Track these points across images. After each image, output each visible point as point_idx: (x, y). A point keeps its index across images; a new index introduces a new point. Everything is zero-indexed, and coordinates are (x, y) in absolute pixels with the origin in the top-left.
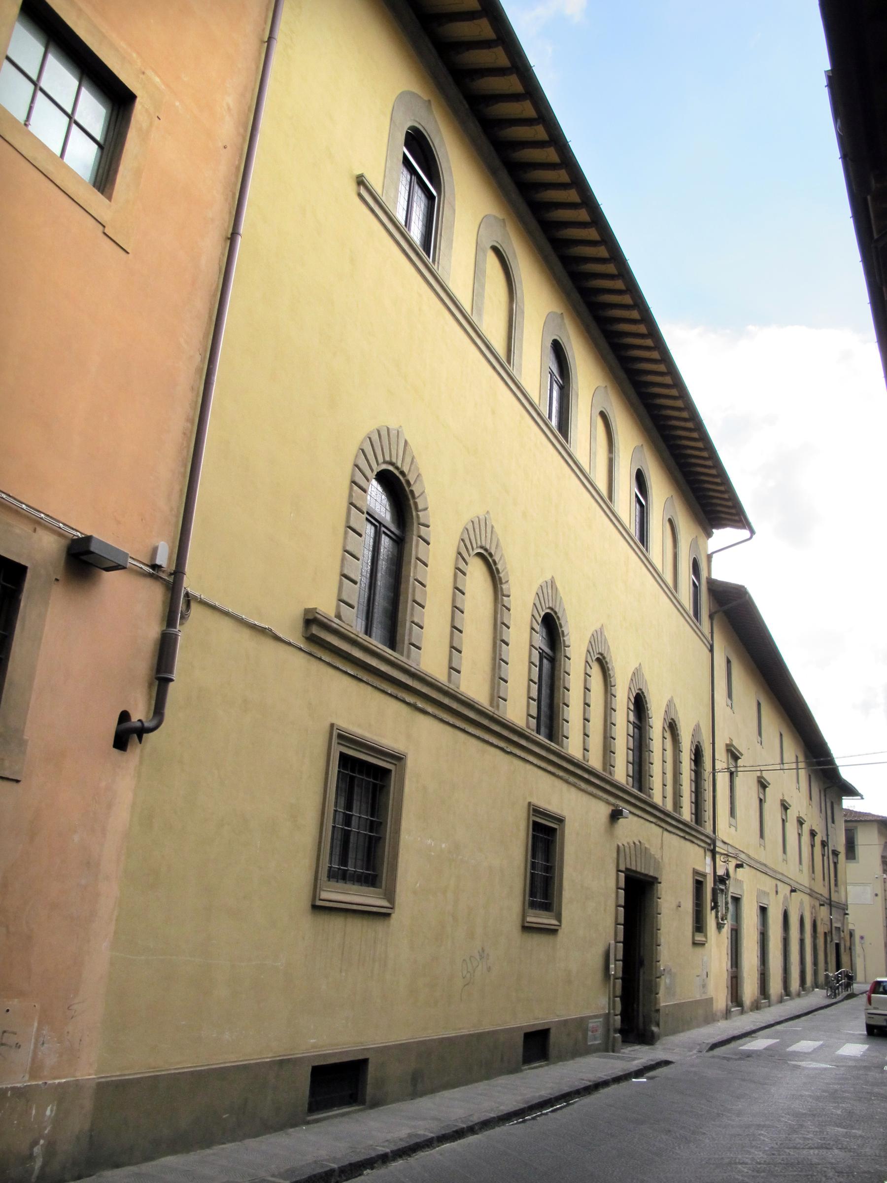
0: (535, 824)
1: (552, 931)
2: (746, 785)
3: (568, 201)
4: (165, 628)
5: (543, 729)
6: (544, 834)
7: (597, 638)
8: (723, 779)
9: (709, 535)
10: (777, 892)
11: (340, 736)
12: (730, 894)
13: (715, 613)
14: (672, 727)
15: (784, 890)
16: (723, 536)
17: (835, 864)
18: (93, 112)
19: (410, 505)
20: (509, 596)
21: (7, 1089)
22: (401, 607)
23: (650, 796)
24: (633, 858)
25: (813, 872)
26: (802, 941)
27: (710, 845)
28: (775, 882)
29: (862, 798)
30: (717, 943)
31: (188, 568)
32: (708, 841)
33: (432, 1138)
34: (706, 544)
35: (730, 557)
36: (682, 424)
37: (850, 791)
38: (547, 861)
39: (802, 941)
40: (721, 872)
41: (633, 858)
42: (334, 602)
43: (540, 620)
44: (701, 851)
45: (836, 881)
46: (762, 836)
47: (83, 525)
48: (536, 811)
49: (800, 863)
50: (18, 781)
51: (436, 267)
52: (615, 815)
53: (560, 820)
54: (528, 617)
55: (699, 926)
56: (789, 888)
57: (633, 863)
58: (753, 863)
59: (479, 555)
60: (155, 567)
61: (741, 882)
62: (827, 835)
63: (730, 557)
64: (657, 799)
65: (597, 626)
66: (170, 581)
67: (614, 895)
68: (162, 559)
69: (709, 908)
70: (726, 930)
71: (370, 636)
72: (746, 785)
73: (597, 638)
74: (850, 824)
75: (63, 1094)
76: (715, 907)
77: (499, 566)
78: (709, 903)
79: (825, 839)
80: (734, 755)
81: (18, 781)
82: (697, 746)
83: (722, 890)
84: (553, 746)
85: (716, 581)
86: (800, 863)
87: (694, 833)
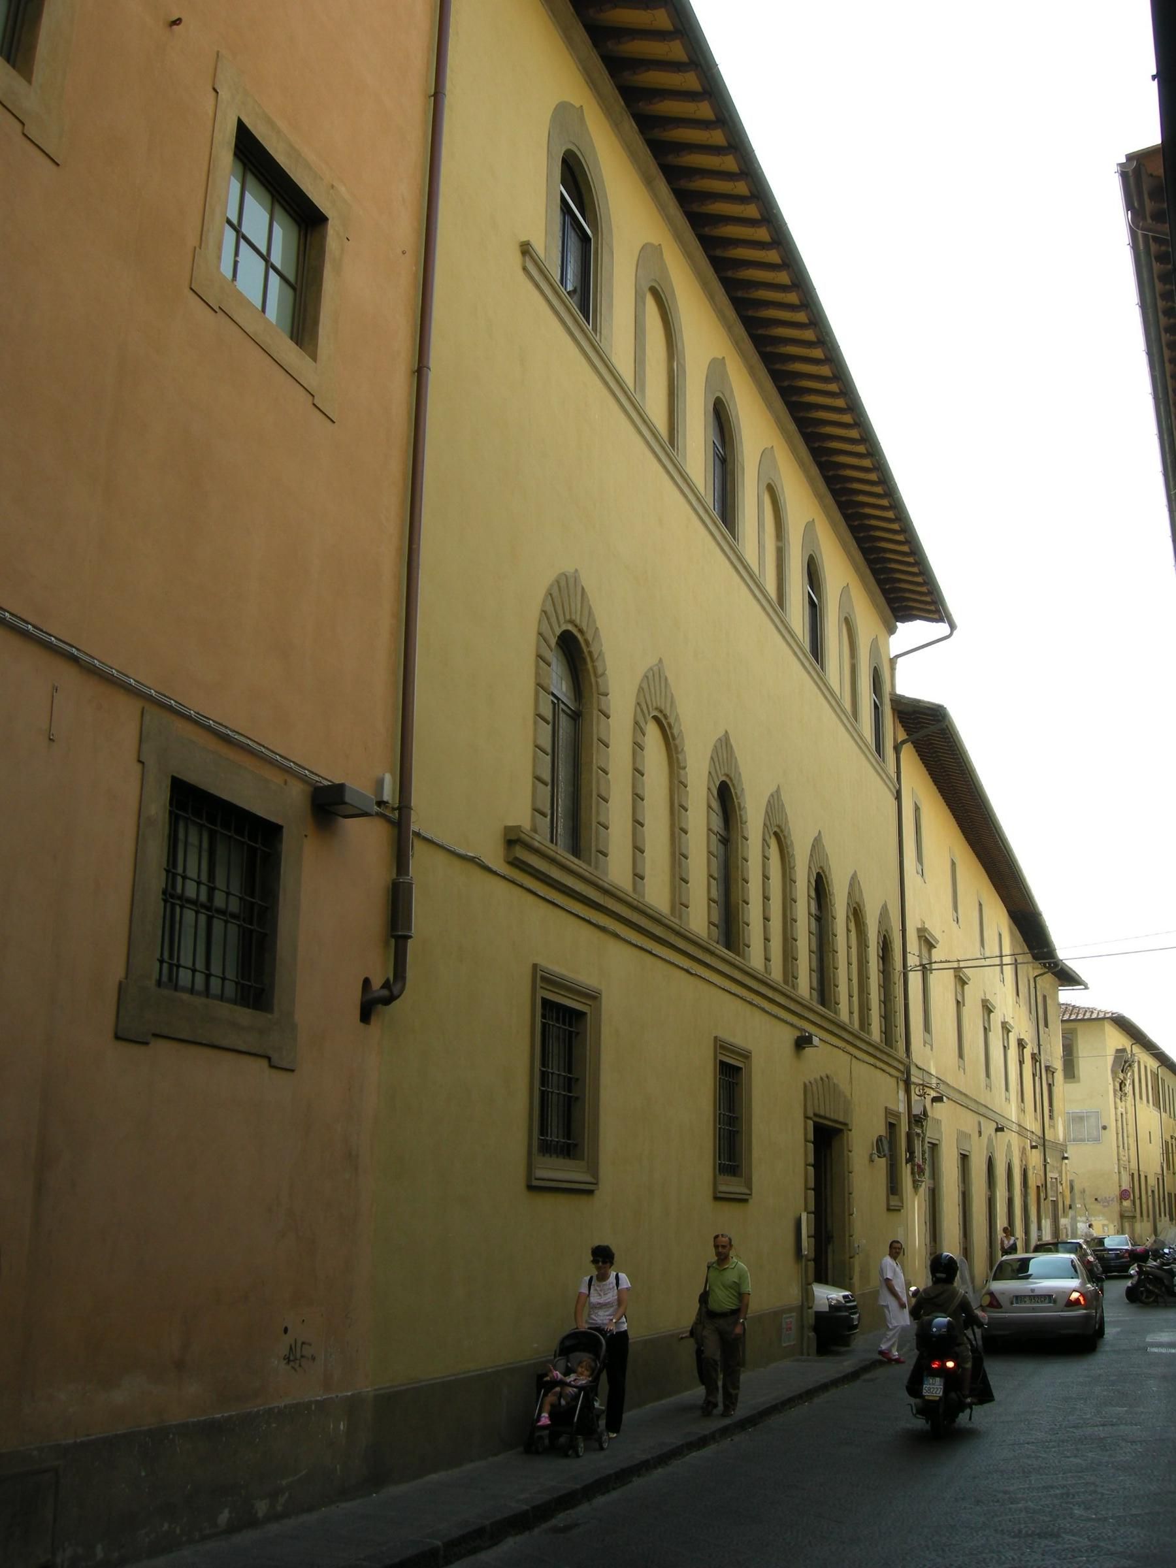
0: (546, 1003)
1: (743, 1200)
2: (942, 983)
3: (721, 169)
4: (394, 876)
5: (561, 841)
6: (731, 1076)
7: (654, 682)
8: (915, 979)
9: (892, 630)
10: (980, 1132)
11: (543, 979)
12: (927, 1140)
13: (903, 742)
14: (857, 914)
15: (989, 1128)
16: (911, 632)
17: (1050, 1086)
18: (281, 241)
19: (588, 671)
20: (607, 695)
21: (310, 1402)
22: (583, 804)
23: (835, 1013)
24: (821, 1099)
25: (1022, 1101)
26: (1010, 1201)
27: (902, 1073)
28: (977, 1118)
29: (1086, 988)
30: (916, 1206)
31: (415, 801)
32: (901, 1067)
33: (609, 1476)
34: (888, 644)
35: (922, 662)
36: (861, 475)
37: (1067, 978)
38: (570, 1072)
39: (1010, 1201)
40: (917, 1110)
41: (821, 1099)
42: (528, 811)
43: (553, 641)
44: (893, 1081)
45: (1051, 1111)
46: (961, 1055)
47: (330, 773)
48: (542, 978)
49: (1007, 1089)
50: (293, 1071)
51: (598, 338)
52: (802, 1043)
53: (593, 997)
54: (532, 637)
55: (894, 1187)
56: (995, 1126)
57: (822, 1106)
58: (956, 1096)
59: (655, 718)
60: (380, 803)
61: (938, 1122)
62: (1039, 1045)
63: (922, 662)
64: (844, 1016)
65: (773, 789)
66: (398, 818)
67: (802, 1151)
68: (387, 796)
69: (904, 1161)
70: (923, 1189)
71: (558, 849)
72: (942, 983)
73: (654, 682)
74: (1067, 1025)
75: (353, 1405)
76: (910, 1160)
77: (675, 731)
78: (903, 1154)
79: (1036, 1051)
80: (928, 943)
81: (293, 1071)
82: (818, 874)
83: (918, 1135)
84: (887, 1049)
85: (903, 697)
86: (1007, 1089)
87: (885, 1058)
